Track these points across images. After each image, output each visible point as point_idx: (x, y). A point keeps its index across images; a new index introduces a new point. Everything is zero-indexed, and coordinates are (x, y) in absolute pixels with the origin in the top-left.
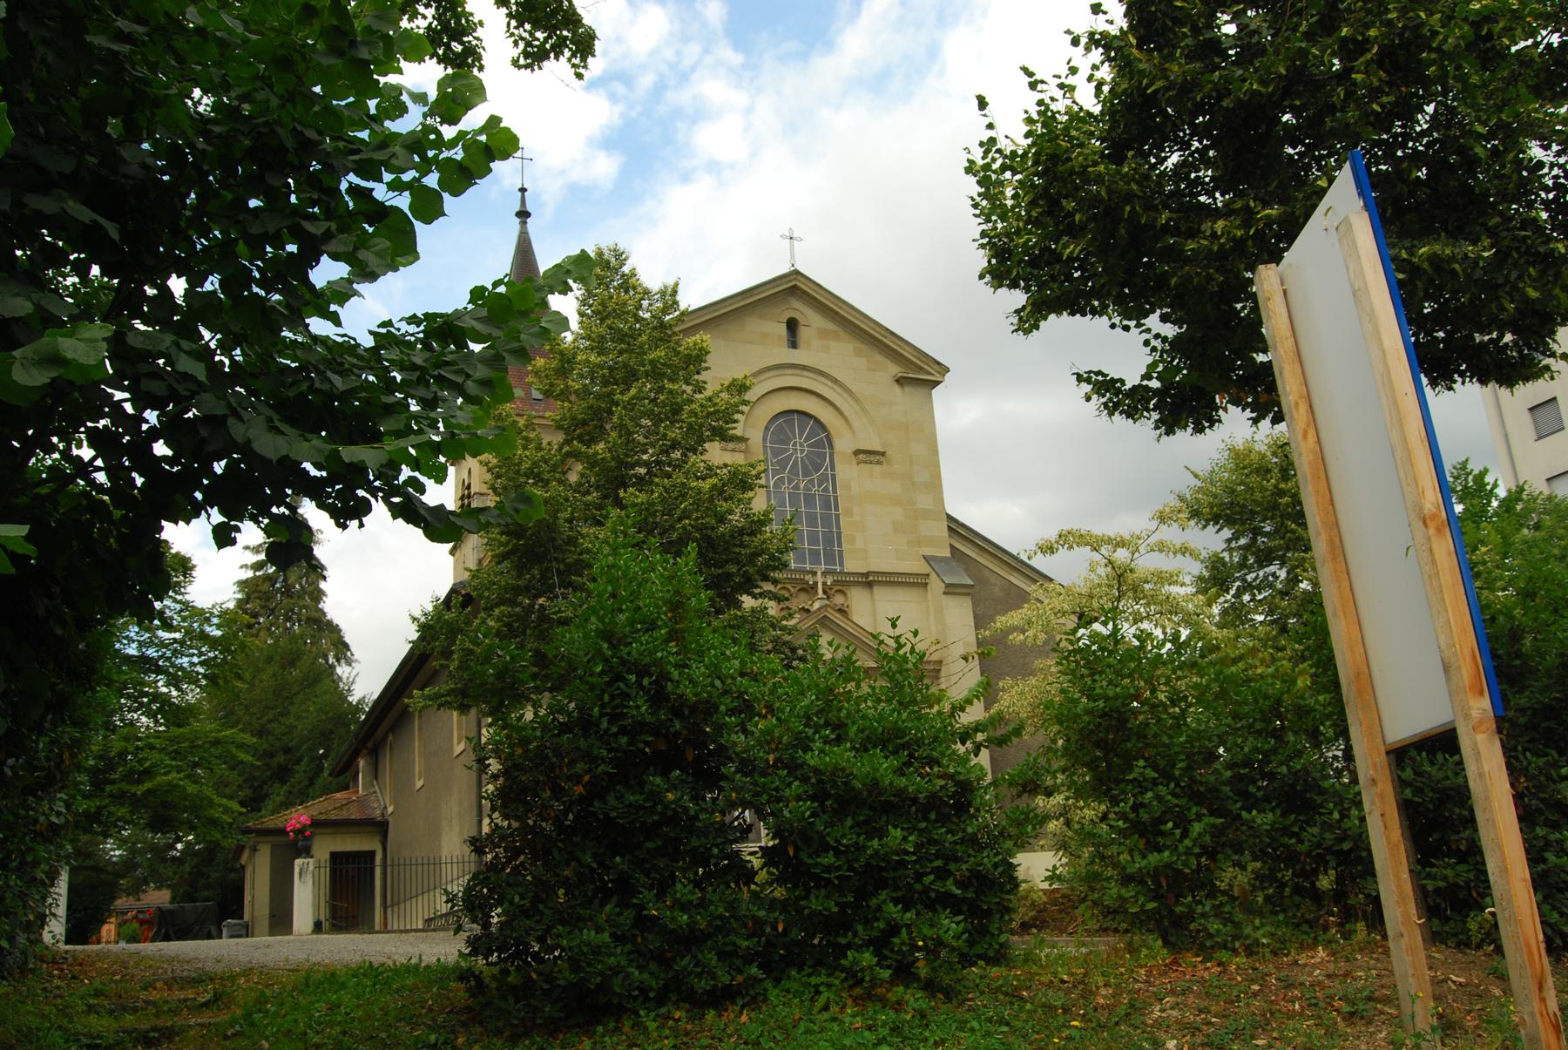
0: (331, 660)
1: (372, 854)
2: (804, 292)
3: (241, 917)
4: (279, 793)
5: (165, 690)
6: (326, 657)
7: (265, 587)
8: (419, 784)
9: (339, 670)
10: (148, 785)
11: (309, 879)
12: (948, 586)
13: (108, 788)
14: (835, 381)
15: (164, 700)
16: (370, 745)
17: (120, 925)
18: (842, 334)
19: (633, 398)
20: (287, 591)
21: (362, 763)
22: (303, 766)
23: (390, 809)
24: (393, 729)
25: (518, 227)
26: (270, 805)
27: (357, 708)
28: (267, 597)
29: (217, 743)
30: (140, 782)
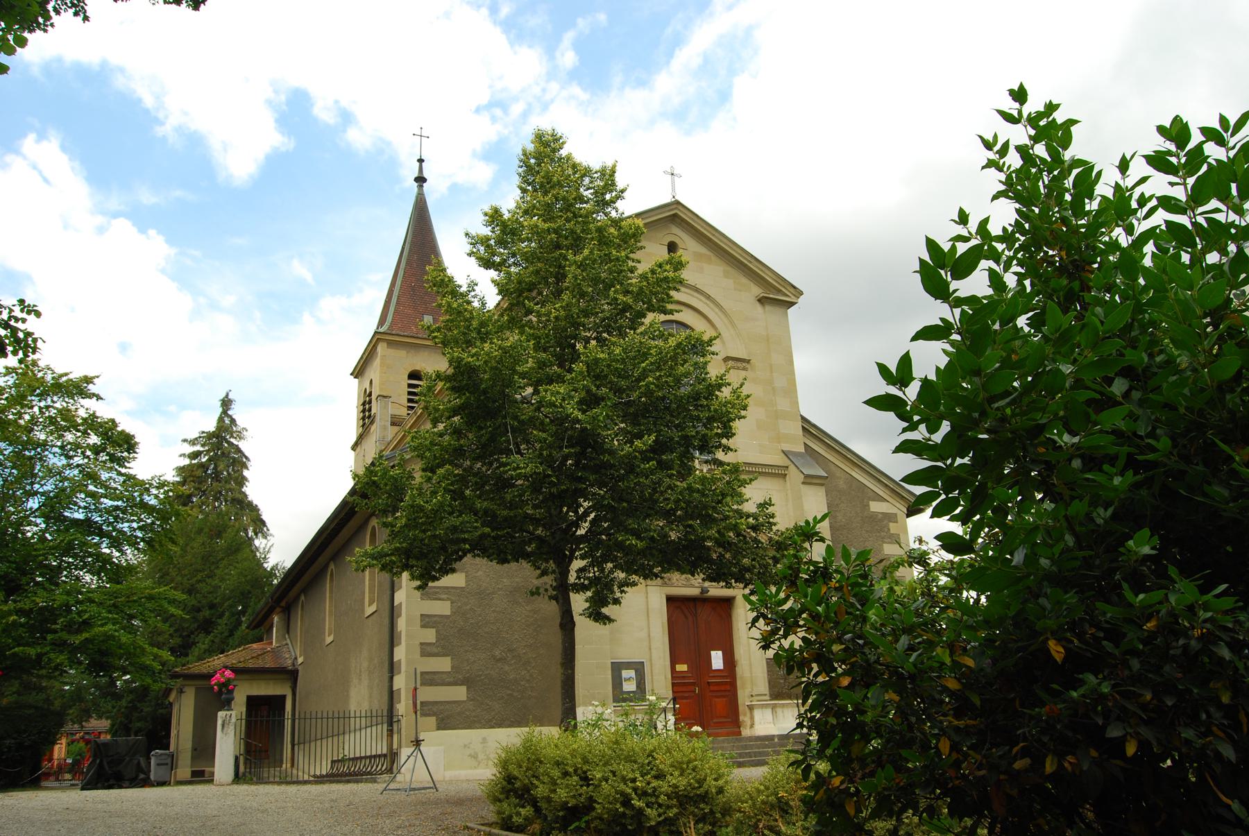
0: (251, 533)
1: (284, 697)
2: (683, 220)
3: (167, 747)
4: (204, 642)
5: (107, 551)
6: (246, 531)
7: (199, 473)
8: (329, 639)
9: (257, 542)
10: (85, 635)
11: (231, 730)
12: (807, 476)
13: (49, 637)
14: (708, 297)
15: (107, 559)
16: (283, 604)
17: (68, 744)
18: (713, 258)
19: (585, 259)
20: (217, 476)
21: (276, 619)
22: (224, 621)
23: (300, 660)
24: (304, 590)
25: (416, 190)
26: (196, 651)
27: (271, 574)
28: (201, 480)
29: (151, 598)
30: (79, 631)
